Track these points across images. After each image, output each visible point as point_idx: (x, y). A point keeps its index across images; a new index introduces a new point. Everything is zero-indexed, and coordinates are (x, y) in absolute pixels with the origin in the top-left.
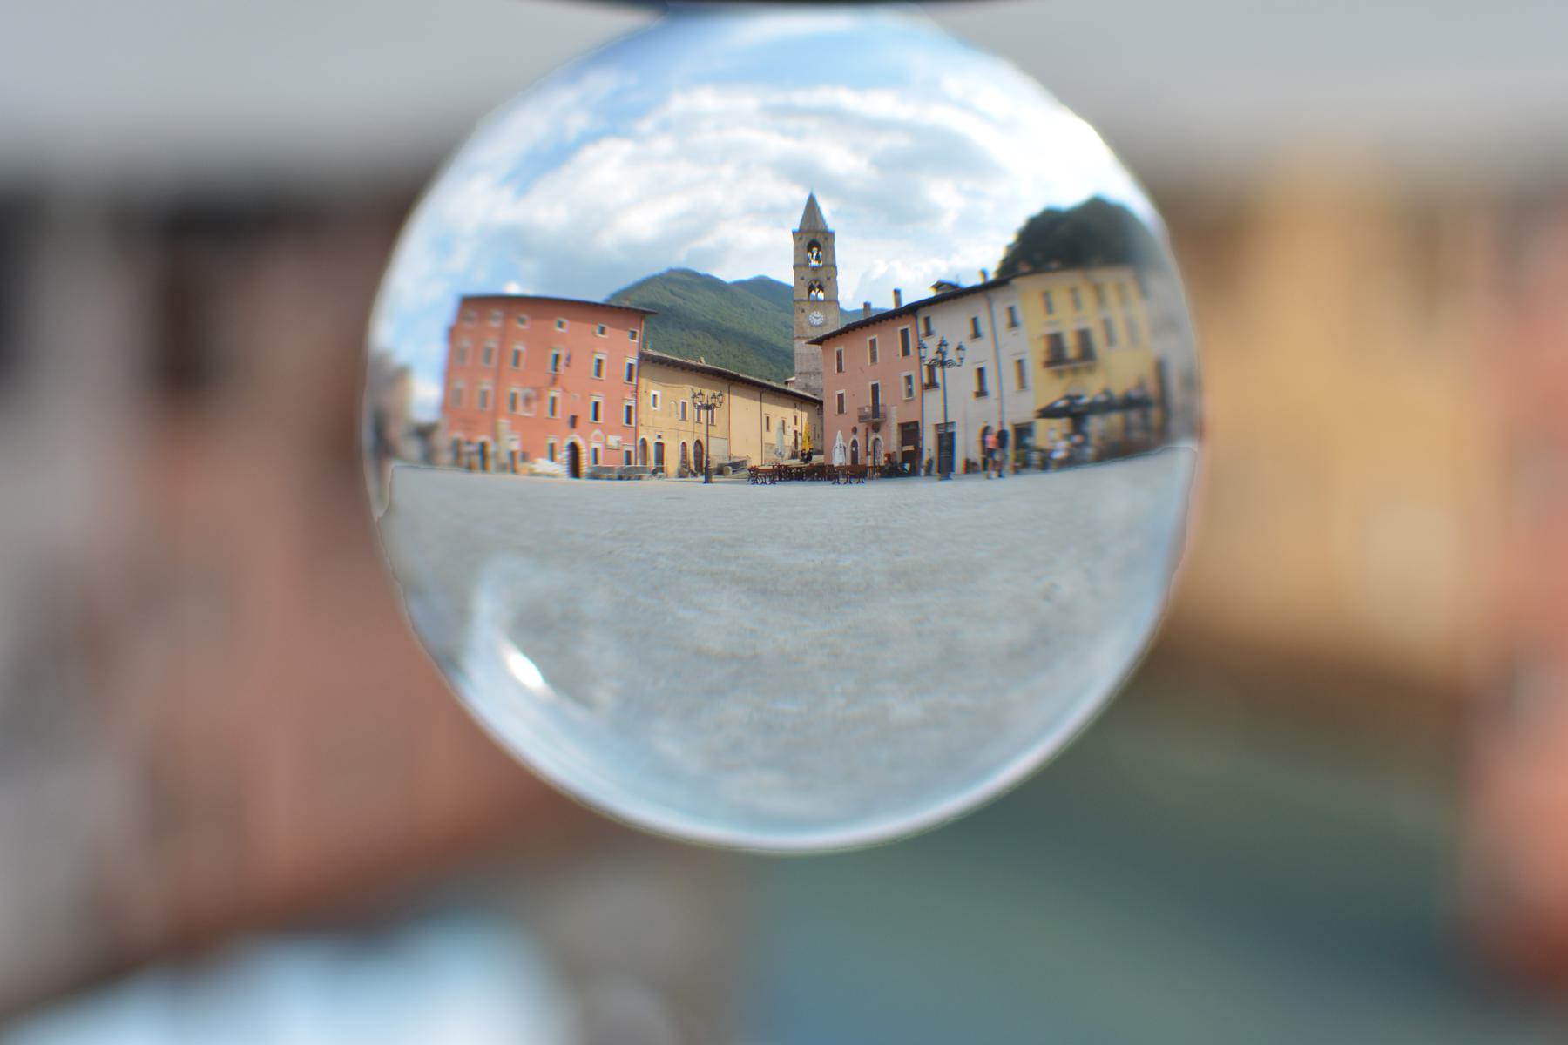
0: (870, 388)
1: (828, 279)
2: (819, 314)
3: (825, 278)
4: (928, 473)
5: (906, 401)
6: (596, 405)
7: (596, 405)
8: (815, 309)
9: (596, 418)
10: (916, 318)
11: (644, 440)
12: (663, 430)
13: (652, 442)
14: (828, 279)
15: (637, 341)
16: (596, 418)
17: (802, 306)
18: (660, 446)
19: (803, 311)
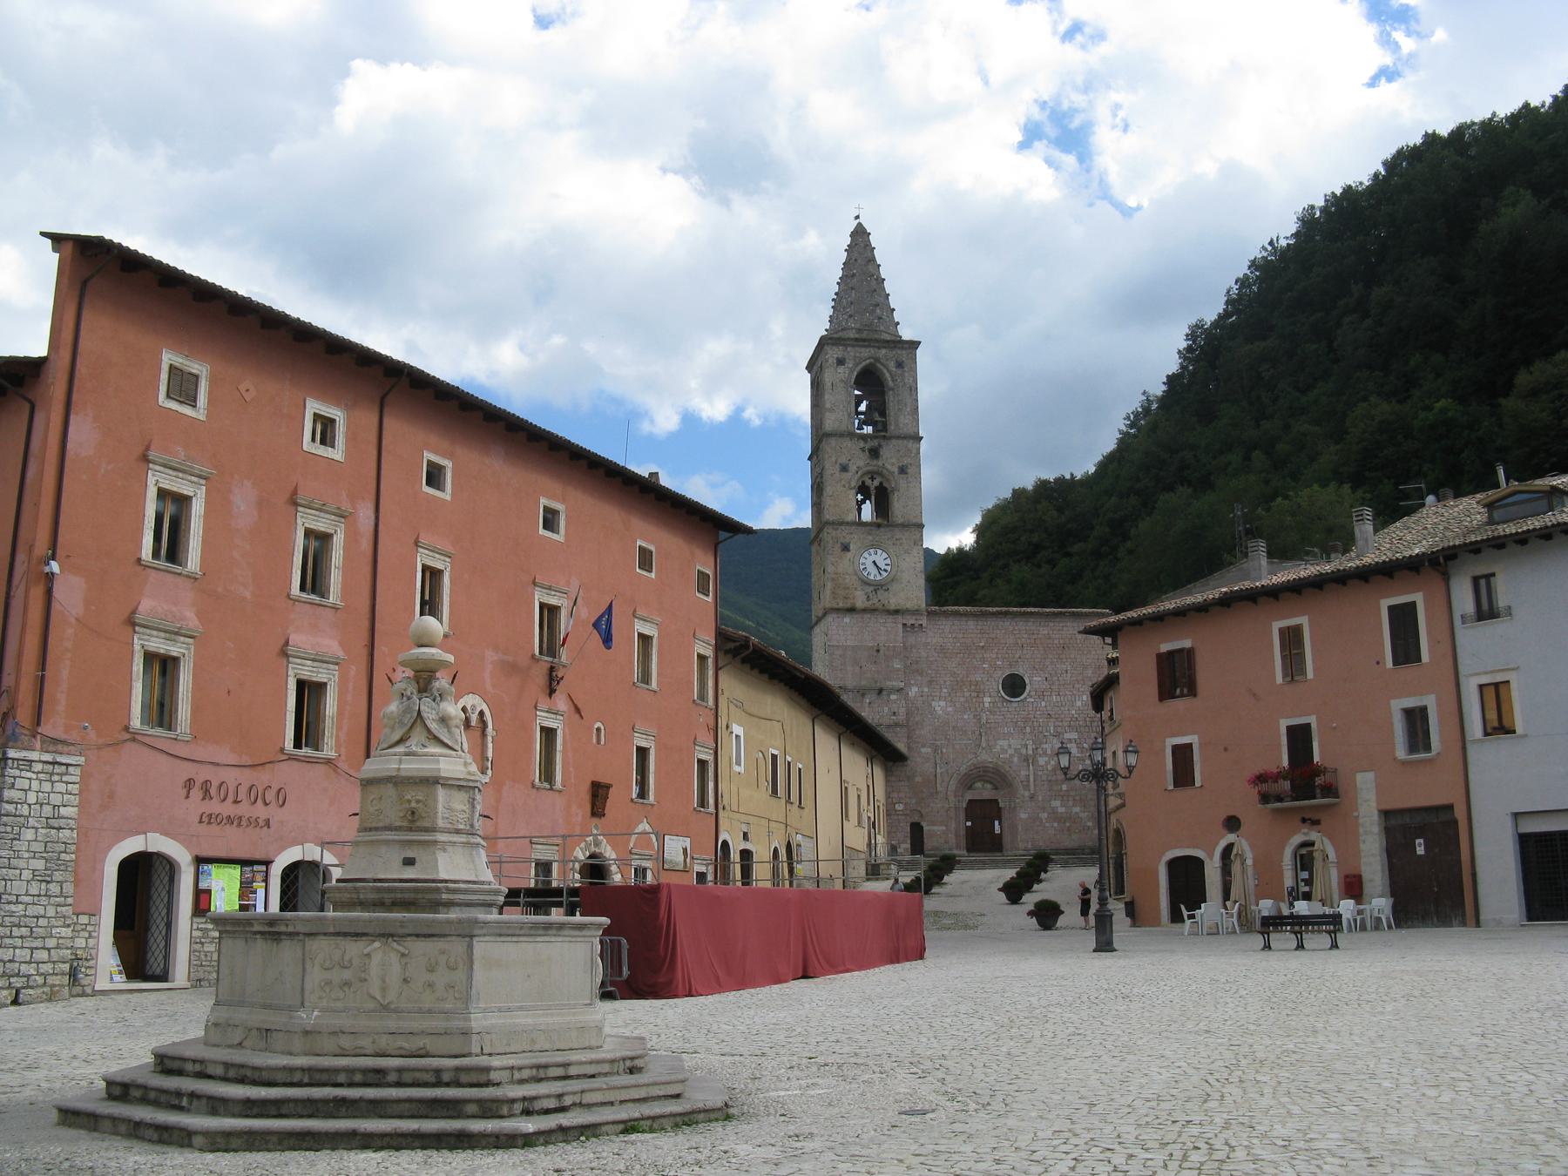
0: (1283, 731)
1: (903, 470)
2: (881, 558)
3: (896, 470)
4: (1350, 930)
5: (1404, 763)
6: (642, 753)
7: (642, 753)
8: (872, 546)
9: (643, 794)
10: (1446, 577)
11: (725, 843)
12: (751, 819)
13: (737, 846)
14: (903, 470)
15: (710, 599)
16: (643, 794)
17: (843, 534)
18: (746, 855)
19: (846, 548)
